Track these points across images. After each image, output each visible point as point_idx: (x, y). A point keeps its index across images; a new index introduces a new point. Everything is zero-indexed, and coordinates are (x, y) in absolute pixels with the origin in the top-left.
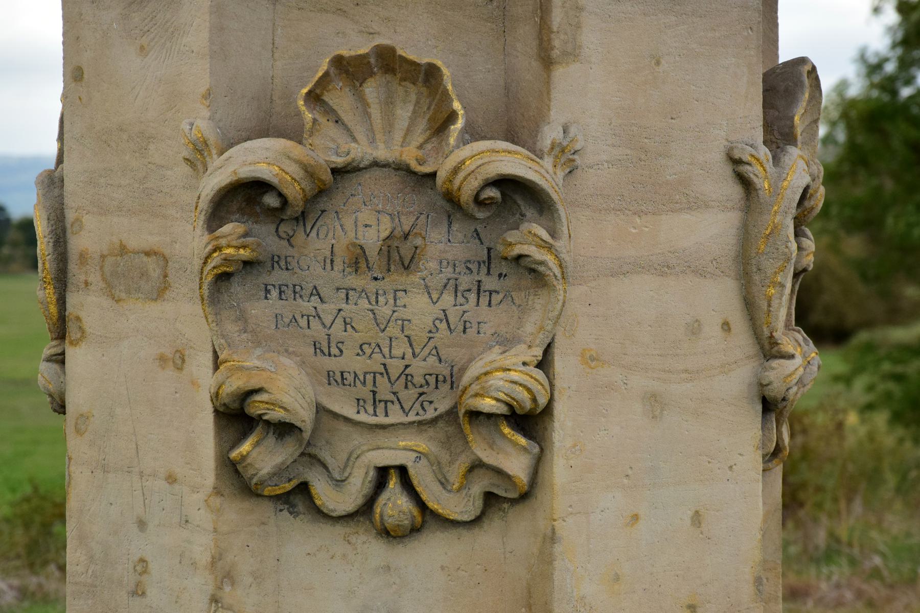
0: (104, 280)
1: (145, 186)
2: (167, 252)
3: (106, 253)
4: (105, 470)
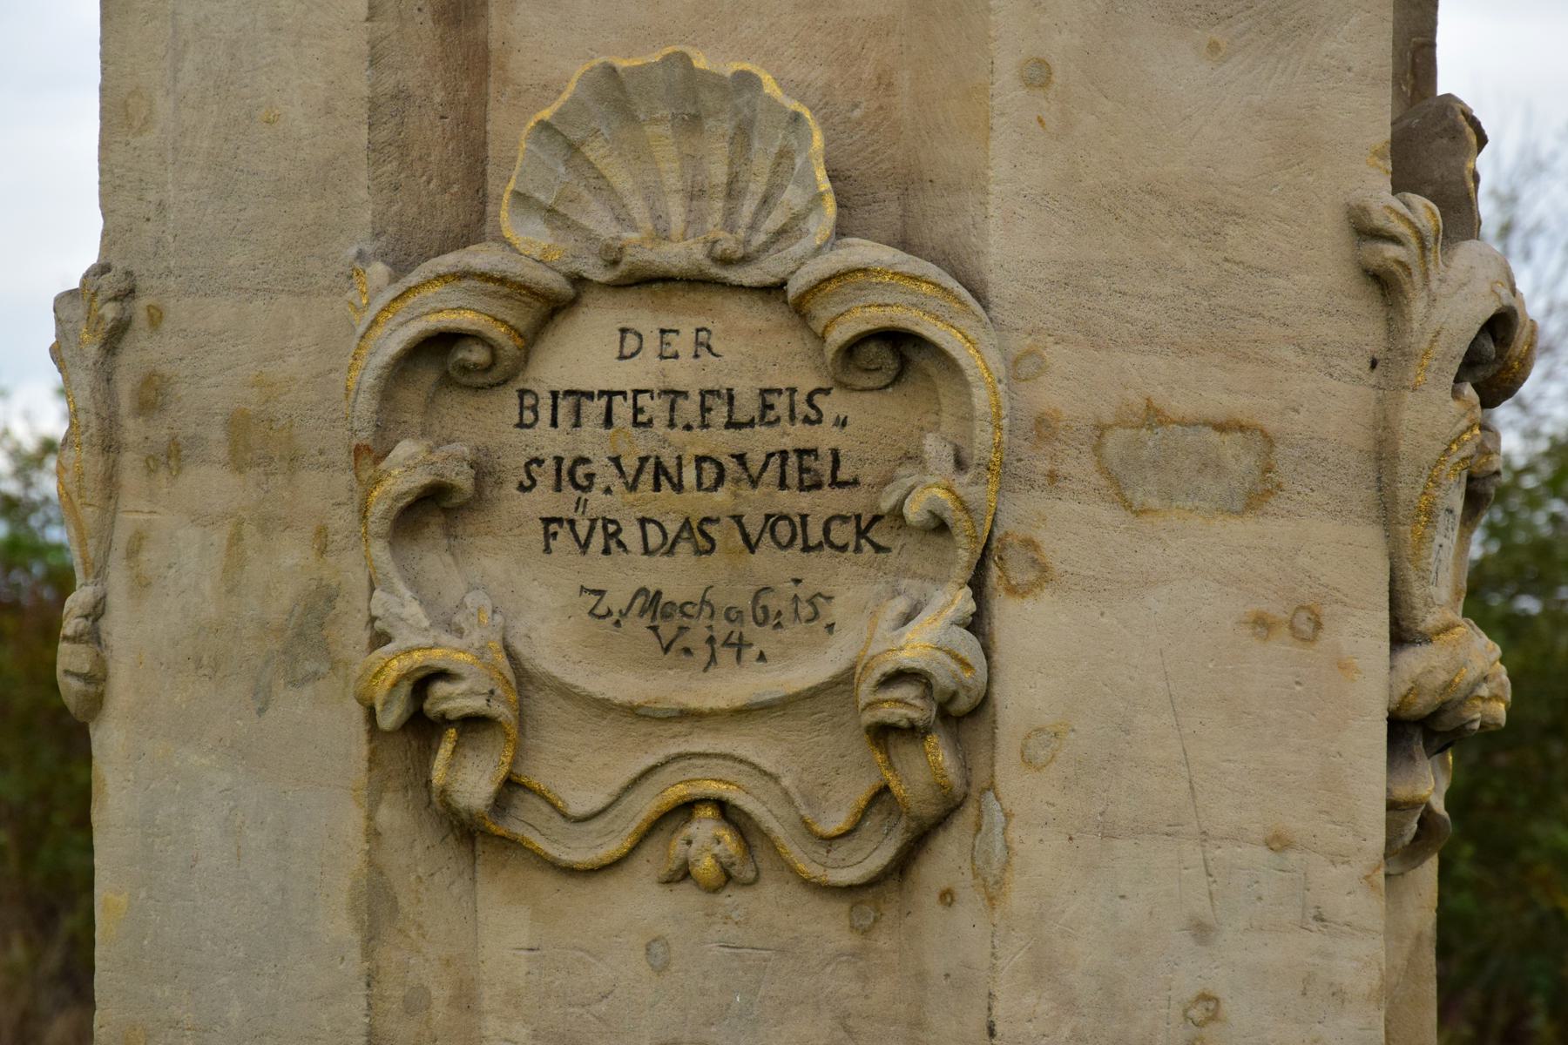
0: (1106, 472)
1: (1214, 301)
2: (1272, 425)
3: (1108, 418)
4: (1108, 833)
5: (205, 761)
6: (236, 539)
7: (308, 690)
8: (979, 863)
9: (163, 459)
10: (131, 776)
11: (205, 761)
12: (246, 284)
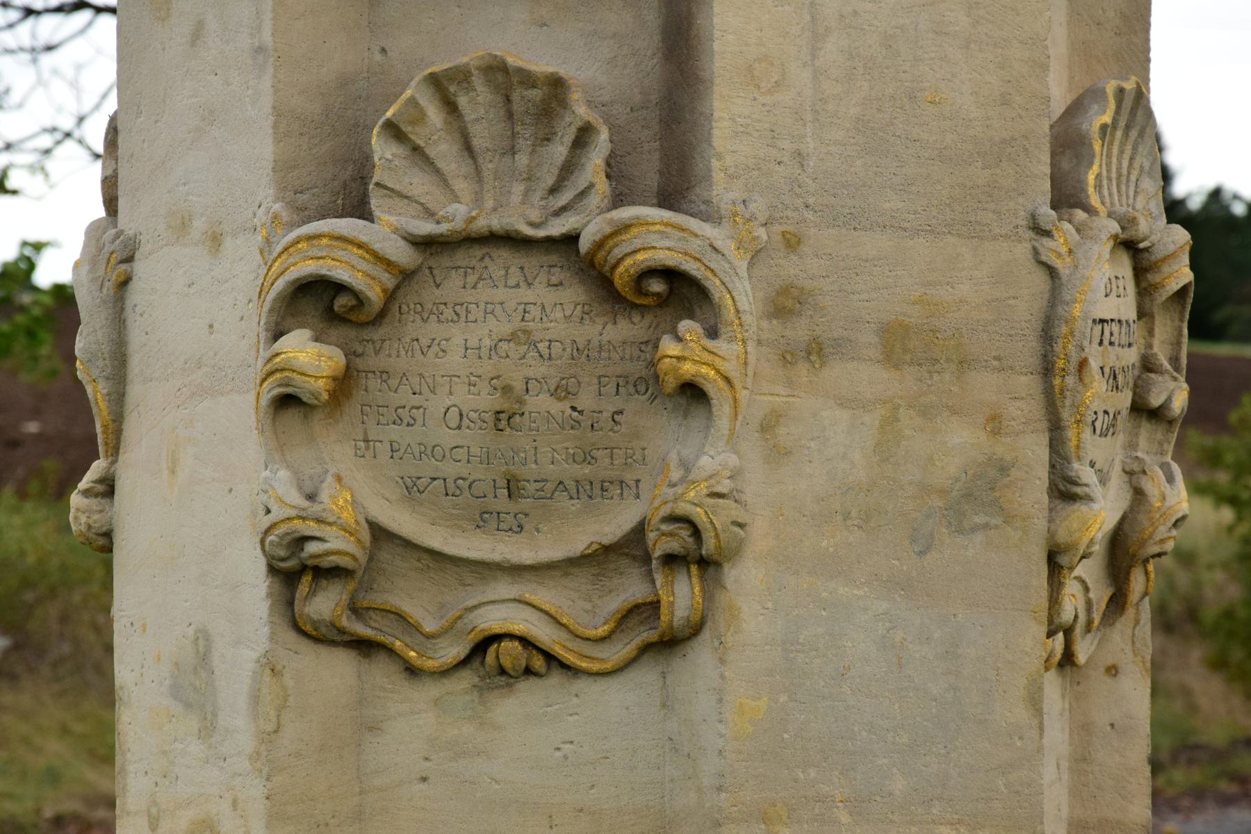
5: (861, 593)
6: (891, 420)
7: (979, 538)
8: (1138, 645)
9: (803, 354)
10: (770, 605)
11: (861, 593)
12: (906, 225)
